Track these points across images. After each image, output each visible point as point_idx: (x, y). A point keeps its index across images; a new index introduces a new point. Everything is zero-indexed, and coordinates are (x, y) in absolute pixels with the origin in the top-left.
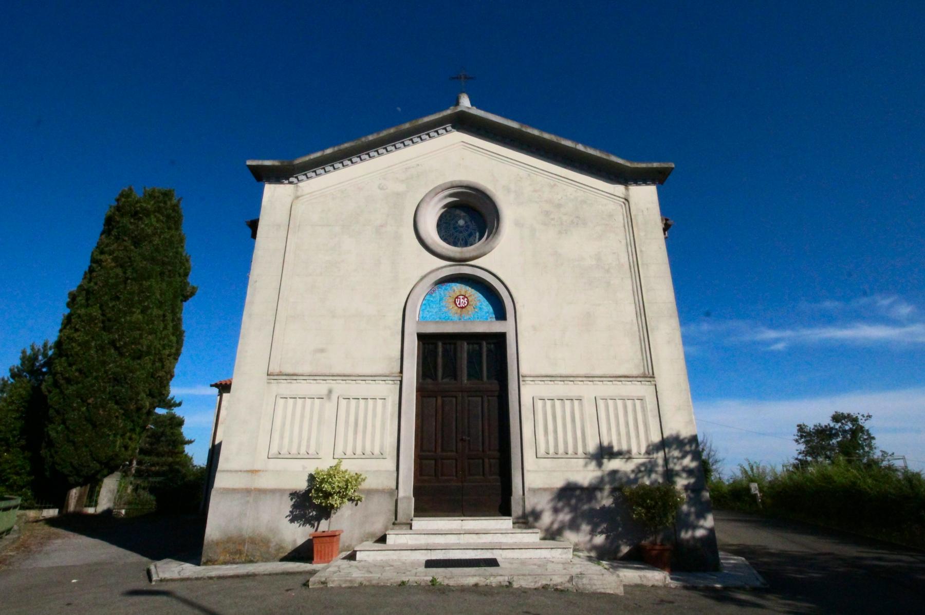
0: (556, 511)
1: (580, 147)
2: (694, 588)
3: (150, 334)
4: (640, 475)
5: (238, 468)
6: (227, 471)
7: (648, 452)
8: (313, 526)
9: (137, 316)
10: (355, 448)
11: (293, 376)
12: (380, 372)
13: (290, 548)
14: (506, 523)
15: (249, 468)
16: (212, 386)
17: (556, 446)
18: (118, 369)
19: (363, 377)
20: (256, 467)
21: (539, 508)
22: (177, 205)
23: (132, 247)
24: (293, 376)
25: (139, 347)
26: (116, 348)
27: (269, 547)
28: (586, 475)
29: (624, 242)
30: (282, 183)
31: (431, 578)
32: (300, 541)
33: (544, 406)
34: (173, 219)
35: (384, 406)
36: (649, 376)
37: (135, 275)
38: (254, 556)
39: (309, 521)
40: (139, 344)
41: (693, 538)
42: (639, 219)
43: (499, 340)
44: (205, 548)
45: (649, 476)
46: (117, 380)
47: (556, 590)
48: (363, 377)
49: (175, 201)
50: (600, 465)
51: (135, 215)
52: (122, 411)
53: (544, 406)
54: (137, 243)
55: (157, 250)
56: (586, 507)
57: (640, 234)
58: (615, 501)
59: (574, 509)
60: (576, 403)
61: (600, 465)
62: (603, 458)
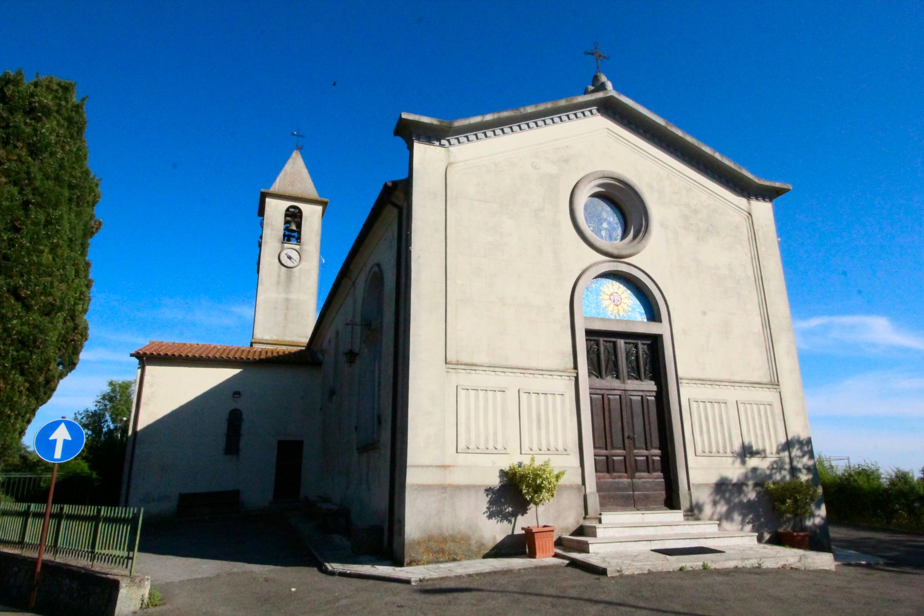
0: (715, 503)
1: (718, 156)
2: (849, 565)
3: (62, 281)
4: (774, 471)
5: (427, 463)
6: (418, 466)
7: (778, 452)
8: (510, 521)
9: (47, 258)
10: (540, 443)
11: (471, 366)
12: (554, 367)
13: (490, 545)
14: (677, 516)
15: (439, 463)
16: (132, 355)
17: (710, 445)
18: (25, 328)
19: (541, 371)
20: (447, 463)
21: (701, 501)
22: (77, 108)
23: (30, 159)
24: (471, 366)
25: (51, 299)
26: (18, 298)
27: (470, 545)
28: (735, 472)
29: (749, 255)
30: (433, 144)
31: (701, 563)
32: (500, 538)
33: (698, 407)
34: (74, 125)
35: (563, 403)
36: (775, 384)
37: (39, 199)
38: (456, 554)
39: (506, 517)
40: (50, 294)
41: (814, 524)
42: (760, 235)
43: (655, 342)
44: (406, 547)
45: (780, 472)
46: (23, 343)
47: (792, 568)
48: (541, 371)
49: (75, 99)
50: (743, 462)
51: (30, 111)
52: (27, 385)
53: (698, 407)
54: (34, 151)
55: (61, 167)
56: (737, 500)
57: (762, 250)
58: (758, 494)
59: (728, 501)
60: (723, 405)
61: (743, 462)
62: (745, 456)
